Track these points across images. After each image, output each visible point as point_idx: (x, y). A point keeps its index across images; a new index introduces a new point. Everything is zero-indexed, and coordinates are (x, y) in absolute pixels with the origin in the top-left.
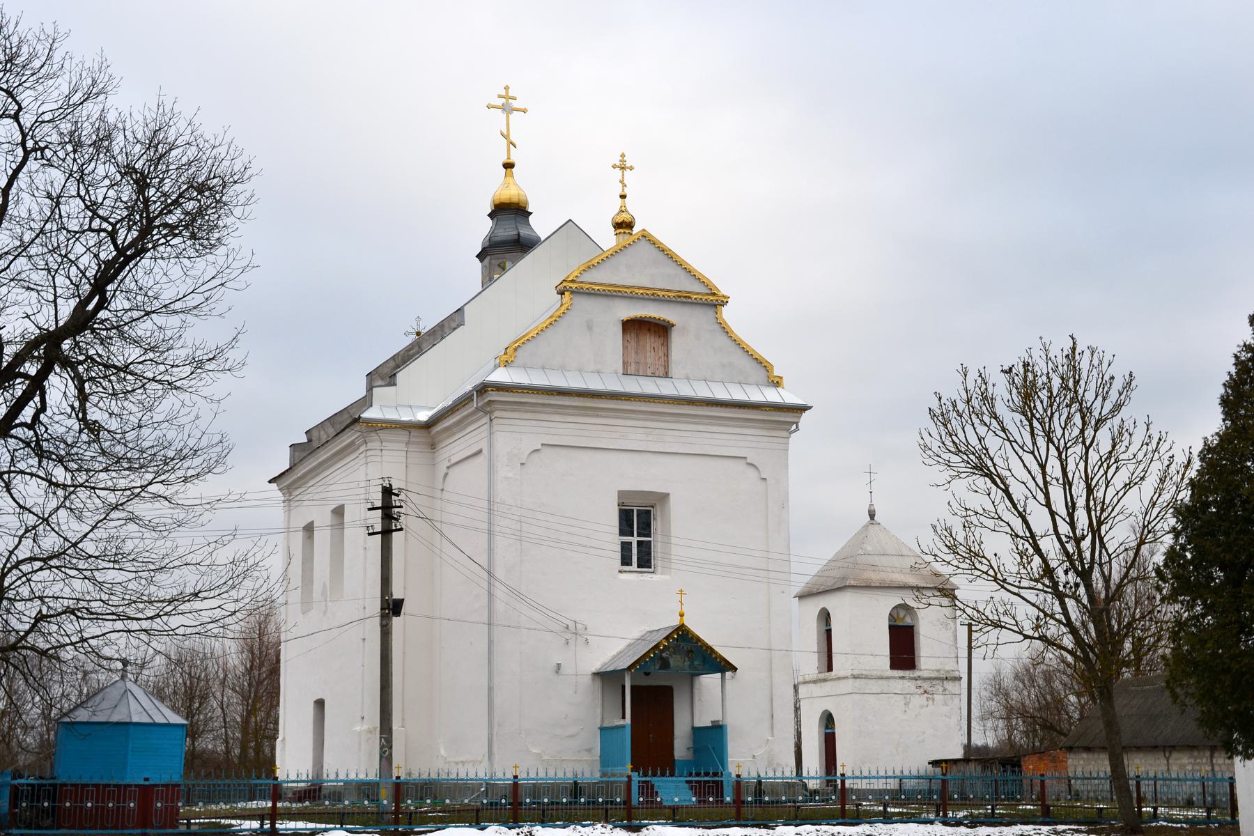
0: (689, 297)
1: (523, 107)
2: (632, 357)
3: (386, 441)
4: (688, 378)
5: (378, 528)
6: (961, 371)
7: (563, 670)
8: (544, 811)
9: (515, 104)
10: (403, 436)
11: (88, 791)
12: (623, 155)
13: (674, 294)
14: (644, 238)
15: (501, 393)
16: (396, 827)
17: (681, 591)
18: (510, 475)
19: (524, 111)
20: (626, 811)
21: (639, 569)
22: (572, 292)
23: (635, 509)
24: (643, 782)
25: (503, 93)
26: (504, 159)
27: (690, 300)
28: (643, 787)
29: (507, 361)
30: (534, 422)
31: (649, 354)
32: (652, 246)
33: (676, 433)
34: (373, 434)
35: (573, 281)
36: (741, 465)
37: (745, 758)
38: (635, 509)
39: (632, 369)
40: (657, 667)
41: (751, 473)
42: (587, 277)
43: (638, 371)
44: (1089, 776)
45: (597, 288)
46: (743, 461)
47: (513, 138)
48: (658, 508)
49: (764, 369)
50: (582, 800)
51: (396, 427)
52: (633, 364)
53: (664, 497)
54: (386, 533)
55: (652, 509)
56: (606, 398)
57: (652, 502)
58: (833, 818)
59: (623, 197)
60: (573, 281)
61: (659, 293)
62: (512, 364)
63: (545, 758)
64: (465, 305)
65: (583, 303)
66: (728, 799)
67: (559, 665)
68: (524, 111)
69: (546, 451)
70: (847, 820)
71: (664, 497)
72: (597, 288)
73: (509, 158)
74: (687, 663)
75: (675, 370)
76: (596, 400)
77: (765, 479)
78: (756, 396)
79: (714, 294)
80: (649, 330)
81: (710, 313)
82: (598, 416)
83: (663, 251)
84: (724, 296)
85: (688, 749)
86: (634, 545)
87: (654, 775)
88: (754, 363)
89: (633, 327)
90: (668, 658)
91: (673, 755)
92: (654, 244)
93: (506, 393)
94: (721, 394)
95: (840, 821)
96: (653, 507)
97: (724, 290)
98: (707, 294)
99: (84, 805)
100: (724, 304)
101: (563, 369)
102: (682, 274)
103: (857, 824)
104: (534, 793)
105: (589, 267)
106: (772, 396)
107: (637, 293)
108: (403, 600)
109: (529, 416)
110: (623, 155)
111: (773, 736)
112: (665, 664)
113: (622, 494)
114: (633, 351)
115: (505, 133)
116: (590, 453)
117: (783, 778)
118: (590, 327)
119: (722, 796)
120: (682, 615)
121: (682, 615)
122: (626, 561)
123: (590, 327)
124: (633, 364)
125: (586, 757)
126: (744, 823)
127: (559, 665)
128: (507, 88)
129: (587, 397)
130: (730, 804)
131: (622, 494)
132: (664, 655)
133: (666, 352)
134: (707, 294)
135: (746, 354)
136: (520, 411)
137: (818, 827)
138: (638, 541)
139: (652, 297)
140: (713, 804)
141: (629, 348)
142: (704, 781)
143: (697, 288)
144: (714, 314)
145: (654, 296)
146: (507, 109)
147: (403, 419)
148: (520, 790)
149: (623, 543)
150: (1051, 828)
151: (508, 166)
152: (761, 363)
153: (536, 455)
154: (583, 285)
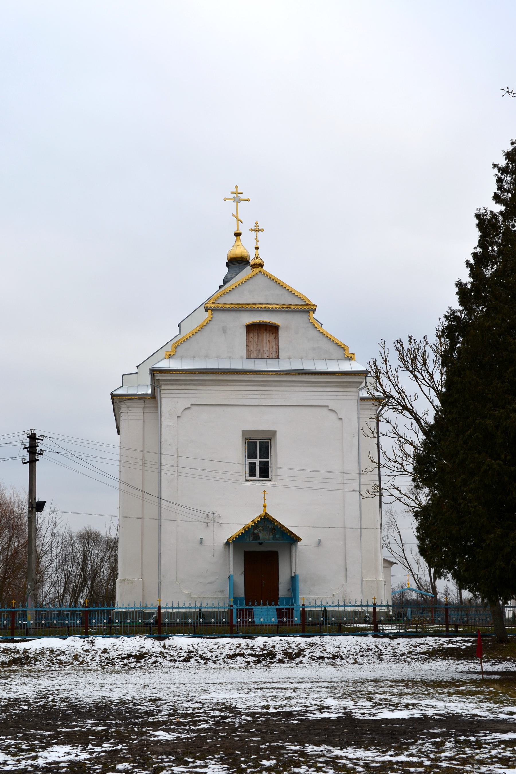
0: (290, 308)
1: (247, 198)
2: (254, 347)
3: (130, 407)
4: (290, 358)
5: (28, 460)
6: (381, 344)
7: (205, 542)
8: (150, 628)
9: (242, 196)
10: (140, 403)
11: (104, 613)
12: (257, 223)
13: (279, 306)
14: (260, 273)
15: (163, 374)
16: (12, 637)
17: (265, 491)
18: (170, 424)
19: (248, 200)
20: (229, 627)
21: (261, 479)
22: (212, 310)
23: (258, 442)
24: (240, 609)
25: (234, 190)
26: (235, 230)
27: (290, 309)
28: (240, 613)
29: (170, 355)
30: (186, 391)
31: (265, 345)
32: (266, 278)
33: (280, 393)
34: (122, 403)
35: (213, 303)
36: (325, 411)
37: (327, 596)
38: (258, 442)
39: (254, 355)
40: (251, 539)
41: (332, 415)
42: (223, 300)
43: (258, 356)
44: (349, 604)
45: (228, 306)
46: (326, 409)
47: (240, 218)
48: (272, 440)
49: (342, 350)
50: (129, 621)
51: (135, 398)
52: (255, 352)
53: (274, 433)
54: (33, 462)
55: (269, 441)
56: (231, 374)
57: (269, 437)
58: (297, 632)
59: (257, 248)
60: (213, 303)
61: (269, 306)
62: (174, 357)
63: (193, 596)
64: (181, 322)
65: (220, 317)
66: (296, 619)
67: (201, 539)
68: (248, 200)
69: (194, 408)
70: (306, 634)
71: (274, 433)
72: (228, 306)
73: (238, 230)
74: (271, 536)
75: (281, 354)
76: (225, 375)
77: (341, 419)
78: (333, 366)
79: (308, 304)
80: (266, 330)
81: (305, 316)
82: (227, 385)
83: (273, 280)
84: (314, 305)
85: (288, 590)
86: (258, 464)
87: (253, 605)
88: (335, 347)
89: (251, 328)
90: (258, 533)
91: (278, 594)
92: (267, 276)
93: (166, 374)
94: (309, 366)
95: (301, 634)
96: (270, 440)
97: (313, 300)
98: (303, 305)
99: (76, 622)
100: (314, 311)
101: (206, 357)
102: (286, 293)
103: (312, 636)
104: (217, 616)
105: (224, 294)
106: (346, 366)
107: (254, 308)
108: (45, 502)
109: (183, 387)
110: (257, 223)
111: (347, 582)
112: (256, 537)
113: (244, 432)
114: (255, 343)
115: (236, 215)
116: (219, 408)
117: (123, 608)
118: (224, 331)
119: (292, 617)
120: (265, 506)
121: (265, 506)
122: (252, 473)
123: (224, 331)
124: (255, 352)
125: (220, 596)
126: (235, 635)
127: (201, 539)
128: (236, 187)
129: (218, 373)
130: (153, 624)
131: (244, 432)
132: (256, 531)
133: (277, 343)
134: (303, 305)
135: (329, 341)
136: (177, 385)
137: (282, 638)
138: (260, 461)
139: (265, 309)
140: (286, 623)
141: (252, 342)
142: (101, 610)
143: (296, 301)
144: (308, 317)
145: (266, 309)
146: (237, 200)
147: (139, 393)
148: (377, 615)
149: (250, 463)
150: (447, 639)
151: (238, 235)
152: (340, 345)
153: (187, 412)
154: (219, 305)
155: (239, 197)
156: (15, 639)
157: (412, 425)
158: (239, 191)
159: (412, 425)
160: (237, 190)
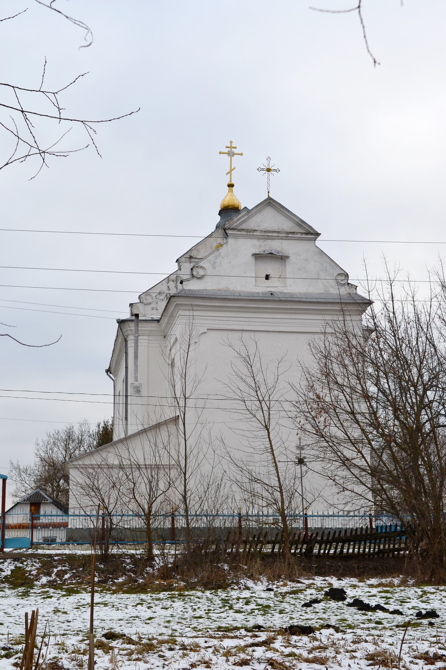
9: (235, 151)
19: (241, 154)
25: (229, 145)
26: (228, 182)
68: (241, 154)
128: (231, 142)
146: (231, 154)
151: (231, 186)
155: (233, 152)
156: (24, 667)
157: (231, 170)
158: (233, 145)
159: (231, 170)
160: (231, 145)
